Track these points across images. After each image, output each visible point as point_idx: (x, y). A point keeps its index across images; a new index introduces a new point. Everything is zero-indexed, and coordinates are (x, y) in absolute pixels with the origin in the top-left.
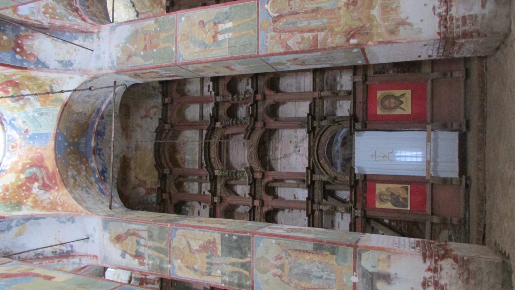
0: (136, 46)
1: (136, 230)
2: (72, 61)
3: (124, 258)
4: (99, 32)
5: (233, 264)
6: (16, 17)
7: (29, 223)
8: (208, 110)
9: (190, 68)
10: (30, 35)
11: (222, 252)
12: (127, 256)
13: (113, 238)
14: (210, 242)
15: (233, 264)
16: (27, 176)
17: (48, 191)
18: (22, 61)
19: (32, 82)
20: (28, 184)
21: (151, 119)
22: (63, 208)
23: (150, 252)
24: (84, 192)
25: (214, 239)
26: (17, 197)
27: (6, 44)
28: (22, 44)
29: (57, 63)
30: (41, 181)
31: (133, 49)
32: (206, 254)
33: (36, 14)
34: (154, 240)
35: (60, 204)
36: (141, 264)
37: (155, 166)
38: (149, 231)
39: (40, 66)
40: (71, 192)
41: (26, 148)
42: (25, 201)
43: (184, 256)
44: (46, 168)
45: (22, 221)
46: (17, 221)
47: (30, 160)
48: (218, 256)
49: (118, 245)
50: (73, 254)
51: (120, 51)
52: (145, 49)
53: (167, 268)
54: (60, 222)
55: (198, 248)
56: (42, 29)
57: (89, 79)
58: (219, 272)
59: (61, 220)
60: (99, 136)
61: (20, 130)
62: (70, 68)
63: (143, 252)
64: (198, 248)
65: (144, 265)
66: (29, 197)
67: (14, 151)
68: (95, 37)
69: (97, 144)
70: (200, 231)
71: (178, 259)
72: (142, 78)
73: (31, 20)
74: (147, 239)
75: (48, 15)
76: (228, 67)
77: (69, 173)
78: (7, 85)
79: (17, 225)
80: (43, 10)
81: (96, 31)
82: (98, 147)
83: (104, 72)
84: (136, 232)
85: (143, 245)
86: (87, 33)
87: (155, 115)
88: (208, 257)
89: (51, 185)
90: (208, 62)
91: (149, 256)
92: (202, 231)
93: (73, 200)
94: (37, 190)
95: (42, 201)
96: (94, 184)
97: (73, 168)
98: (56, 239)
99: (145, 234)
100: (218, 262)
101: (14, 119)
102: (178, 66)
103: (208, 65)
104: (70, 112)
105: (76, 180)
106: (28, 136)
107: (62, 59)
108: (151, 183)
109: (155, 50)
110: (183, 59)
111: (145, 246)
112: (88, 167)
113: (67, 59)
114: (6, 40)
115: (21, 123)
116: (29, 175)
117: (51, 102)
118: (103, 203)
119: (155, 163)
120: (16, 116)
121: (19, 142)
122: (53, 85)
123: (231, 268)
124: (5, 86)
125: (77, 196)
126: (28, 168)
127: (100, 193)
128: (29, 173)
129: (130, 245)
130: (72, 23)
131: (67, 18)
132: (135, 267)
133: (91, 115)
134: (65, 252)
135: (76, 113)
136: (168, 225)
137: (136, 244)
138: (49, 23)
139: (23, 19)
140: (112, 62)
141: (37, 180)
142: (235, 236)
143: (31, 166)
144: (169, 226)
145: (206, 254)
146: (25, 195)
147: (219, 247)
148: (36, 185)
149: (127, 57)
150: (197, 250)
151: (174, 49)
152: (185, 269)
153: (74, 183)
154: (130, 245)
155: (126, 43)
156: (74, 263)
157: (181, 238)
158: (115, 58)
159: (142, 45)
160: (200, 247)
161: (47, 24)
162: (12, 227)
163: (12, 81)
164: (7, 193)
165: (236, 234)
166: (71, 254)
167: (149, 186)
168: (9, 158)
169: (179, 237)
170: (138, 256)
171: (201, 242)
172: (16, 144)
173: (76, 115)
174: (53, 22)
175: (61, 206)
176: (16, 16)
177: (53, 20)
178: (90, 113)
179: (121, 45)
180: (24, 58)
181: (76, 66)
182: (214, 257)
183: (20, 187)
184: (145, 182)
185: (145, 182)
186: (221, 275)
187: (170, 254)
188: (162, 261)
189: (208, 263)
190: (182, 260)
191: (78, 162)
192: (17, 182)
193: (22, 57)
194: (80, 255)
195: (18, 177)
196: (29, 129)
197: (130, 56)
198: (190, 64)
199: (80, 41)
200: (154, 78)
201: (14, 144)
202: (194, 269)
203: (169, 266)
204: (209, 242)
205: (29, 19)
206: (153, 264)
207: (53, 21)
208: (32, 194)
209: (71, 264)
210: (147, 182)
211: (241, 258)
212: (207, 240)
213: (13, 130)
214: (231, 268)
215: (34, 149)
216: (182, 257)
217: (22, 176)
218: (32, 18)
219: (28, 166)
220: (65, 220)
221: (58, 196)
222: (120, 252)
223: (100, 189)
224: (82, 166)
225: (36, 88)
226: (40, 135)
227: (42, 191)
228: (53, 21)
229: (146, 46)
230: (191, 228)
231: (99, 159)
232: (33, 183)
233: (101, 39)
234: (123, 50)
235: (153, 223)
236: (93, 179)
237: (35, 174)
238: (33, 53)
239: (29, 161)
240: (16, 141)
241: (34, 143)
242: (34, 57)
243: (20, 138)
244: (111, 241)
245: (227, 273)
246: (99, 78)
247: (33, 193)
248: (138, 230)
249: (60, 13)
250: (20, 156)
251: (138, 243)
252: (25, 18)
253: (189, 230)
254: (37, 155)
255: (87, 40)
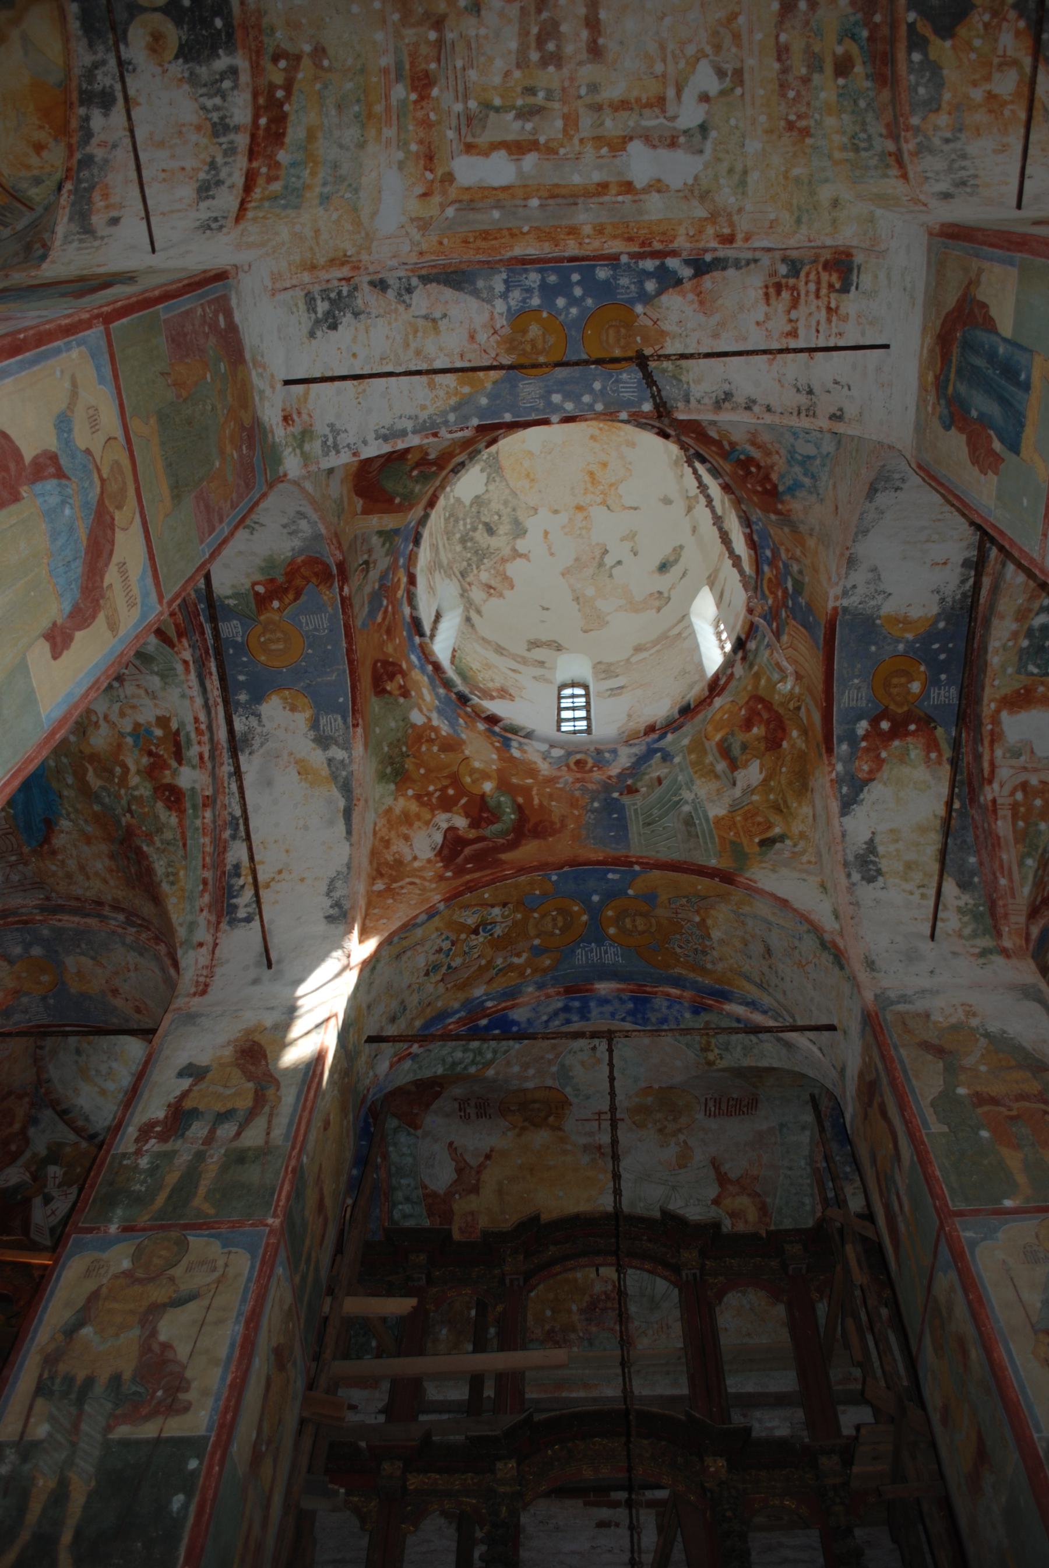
0: (983, 1068)
1: (272, 1108)
2: (880, 879)
3: (181, 1074)
4: (1005, 952)
5: (60, 1496)
6: (988, 707)
7: (336, 793)
8: (774, 1425)
9: (946, 1280)
10: (940, 755)
11: (125, 1443)
12: (186, 1083)
13: (257, 1037)
14: (178, 1389)
15: (60, 1496)
16: (488, 799)
17: (439, 854)
18: (851, 738)
19: (790, 783)
20: (463, 801)
21: (716, 1202)
22: (380, 894)
23: (184, 1158)
24: (432, 958)
25: (186, 1408)
26: (422, 771)
27: (894, 691)
28: (908, 733)
29: (867, 836)
30: (472, 834)
31: (968, 1061)
32: (127, 1375)
33: (1014, 762)
34: (224, 1168)
35: (394, 885)
36: (146, 1132)
37: (536, 1218)
38: (264, 1152)
39: (845, 790)
40: (432, 913)
41: (577, 793)
42: (410, 792)
43: (140, 1281)
44: (513, 845)
45: (344, 773)
46: (343, 761)
47: (541, 804)
48: (109, 1429)
49: (228, 1052)
50: (224, 926)
51: (953, 1020)
52: (980, 1099)
53: (110, 1221)
54: (332, 881)
55: (162, 1337)
56: (967, 783)
57: (827, 937)
58: (41, 1430)
59: (339, 884)
60: (631, 1005)
61: (632, 775)
62: (856, 877)
63: (189, 1133)
64: (162, 1337)
65: (137, 1141)
66: (423, 804)
67: (568, 765)
68: (986, 942)
69: (604, 1001)
70: (232, 1345)
71: (136, 1257)
72: (866, 1116)
73: (992, 750)
74: (237, 1144)
75: (1019, 796)
76: (982, 1455)
77: (496, 911)
78: (768, 722)
79: (330, 761)
80: (1034, 781)
81: (1007, 943)
82: (592, 1004)
83: (863, 976)
84: (267, 1109)
85: (212, 1131)
86: (989, 916)
87: (732, 1215)
88: (116, 1380)
89: (460, 860)
90: (988, 1350)
91: (169, 1156)
92: (229, 1358)
93: (405, 919)
94: (445, 826)
95: (407, 838)
96: (461, 996)
97: (515, 923)
98: (280, 872)
99: (253, 1137)
100: (84, 1427)
101: (667, 757)
102: (942, 1227)
103: (975, 1354)
104: (705, 898)
105: (476, 932)
106: (616, 795)
107: (881, 850)
108: (472, 1213)
109: (985, 1134)
110: (973, 1244)
111: (209, 1140)
112: (522, 974)
113: (884, 865)
114: (908, 692)
115: (655, 775)
116: (492, 803)
117: (732, 843)
118: (393, 1019)
119: (545, 1217)
120: (677, 760)
121: (597, 775)
122: (788, 842)
123: (44, 1483)
124: (765, 716)
125: (419, 932)
126: (514, 801)
127: (429, 1013)
128: (499, 803)
129: (221, 1089)
130: (1015, 867)
131: (1029, 855)
132: (140, 1108)
133: (703, 970)
134: (234, 901)
135: (703, 920)
136: (275, 1216)
137: (223, 1110)
138: (994, 801)
139: (989, 727)
140: (903, 999)
141: (474, 824)
142: (186, 1506)
143: (519, 809)
144: (270, 1221)
145: (127, 1375)
146: (429, 794)
147: (149, 1430)
148: (461, 822)
149: (936, 1041)
150: (154, 1333)
151: (1008, 1203)
152: (90, 1286)
153: (463, 927)
154: (221, 1089)
155: (987, 1035)
156: (192, 926)
157: (214, 1269)
158: (919, 1006)
159: (996, 1089)
160: (166, 1346)
161: (990, 797)
162: (325, 748)
163: (784, 730)
164: (435, 749)
165: (193, 1508)
166: (225, 920)
167: (462, 1205)
168: (545, 756)
169: (220, 1263)
170: (180, 1116)
171: (182, 1351)
172: (591, 771)
173: (697, 919)
174: (1000, 813)
175: (388, 889)
176: (993, 706)
177: (1009, 813)
178: (709, 966)
179: (974, 1022)
180: (864, 744)
181: (867, 892)
182: (109, 1406)
183: (455, 780)
184: (476, 1190)
185: (476, 1190)
186: (28, 1438)
187: (162, 1227)
188: (139, 1200)
189: (90, 1381)
190: (127, 1274)
191: (537, 942)
192: (472, 771)
193: (865, 738)
194: (216, 945)
195: (486, 776)
196: (638, 797)
197: (939, 1051)
198: (960, 1272)
199: (958, 898)
200: (874, 1162)
201: (590, 765)
202: (80, 1324)
203: (113, 1229)
204: (178, 1384)
205: (992, 742)
206: (136, 1168)
207: (1005, 812)
208: (432, 810)
209: (189, 918)
210: (473, 1197)
211: (78, 1534)
212: (188, 1374)
213: (633, 760)
214: (44, 1483)
215: (576, 812)
216: (140, 1274)
217: (488, 787)
218: (999, 753)
219: (520, 800)
220: (336, 895)
221: (424, 879)
222: (203, 1059)
223: (443, 1015)
224: (525, 956)
225: (772, 797)
226: (622, 825)
227: (439, 838)
228: (1005, 812)
229: (994, 1101)
230: (247, 1308)
231: (550, 1009)
232: (467, 815)
233: (982, 961)
234: (956, 1028)
235: (293, 1163)
236: (478, 992)
237: (495, 817)
238: (885, 767)
239: (536, 801)
240: (600, 768)
241: (594, 811)
242: (871, 772)
243: (610, 777)
244: (249, 1032)
245: (27, 1467)
246: (837, 969)
247: (434, 816)
248: (271, 1115)
249: (1039, 833)
250: (551, 781)
251: (223, 1117)
252: (992, 733)
253: (243, 1300)
254: (557, 820)
255: (966, 919)
